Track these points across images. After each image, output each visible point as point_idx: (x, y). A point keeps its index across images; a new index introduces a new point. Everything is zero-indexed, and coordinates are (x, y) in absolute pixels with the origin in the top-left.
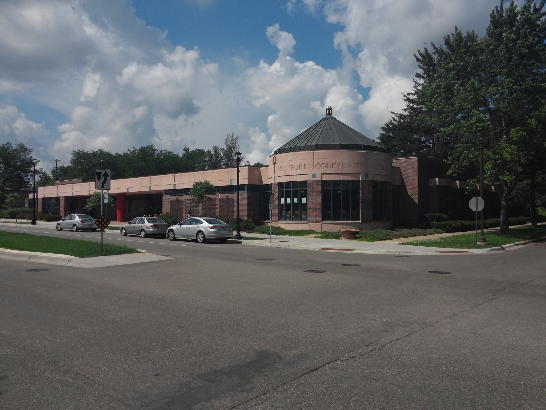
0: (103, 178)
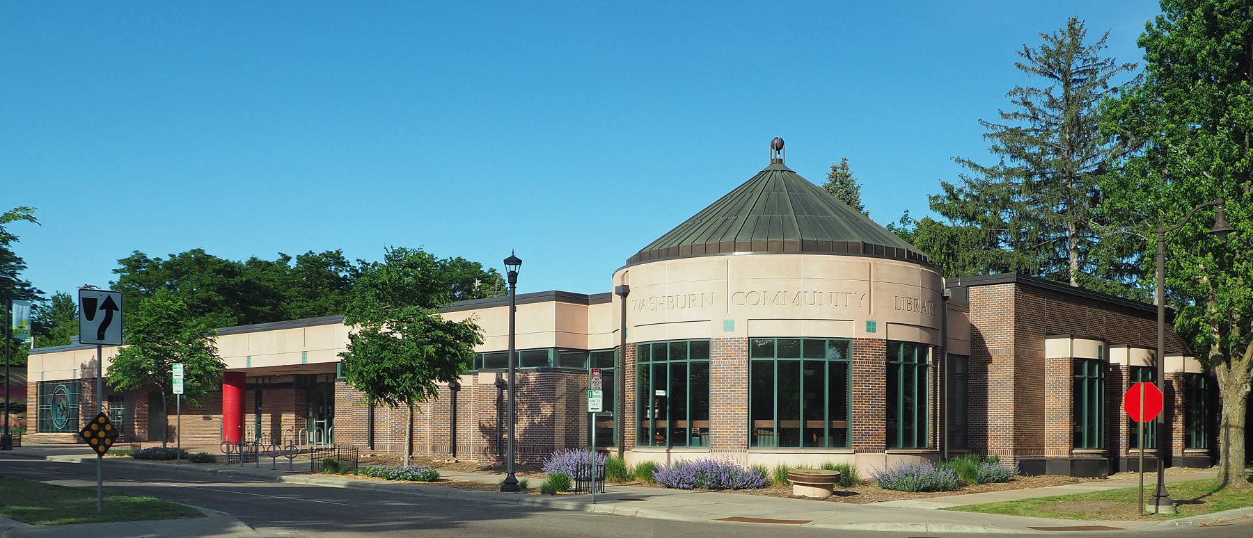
0: (100, 315)
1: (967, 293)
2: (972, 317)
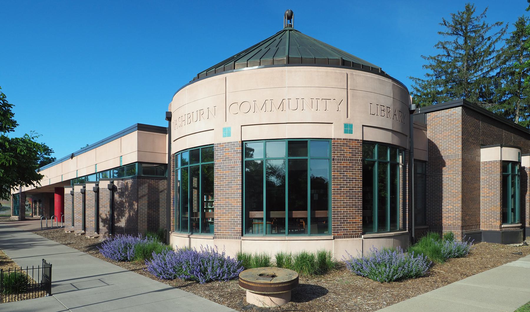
1: (425, 119)
2: (429, 134)
